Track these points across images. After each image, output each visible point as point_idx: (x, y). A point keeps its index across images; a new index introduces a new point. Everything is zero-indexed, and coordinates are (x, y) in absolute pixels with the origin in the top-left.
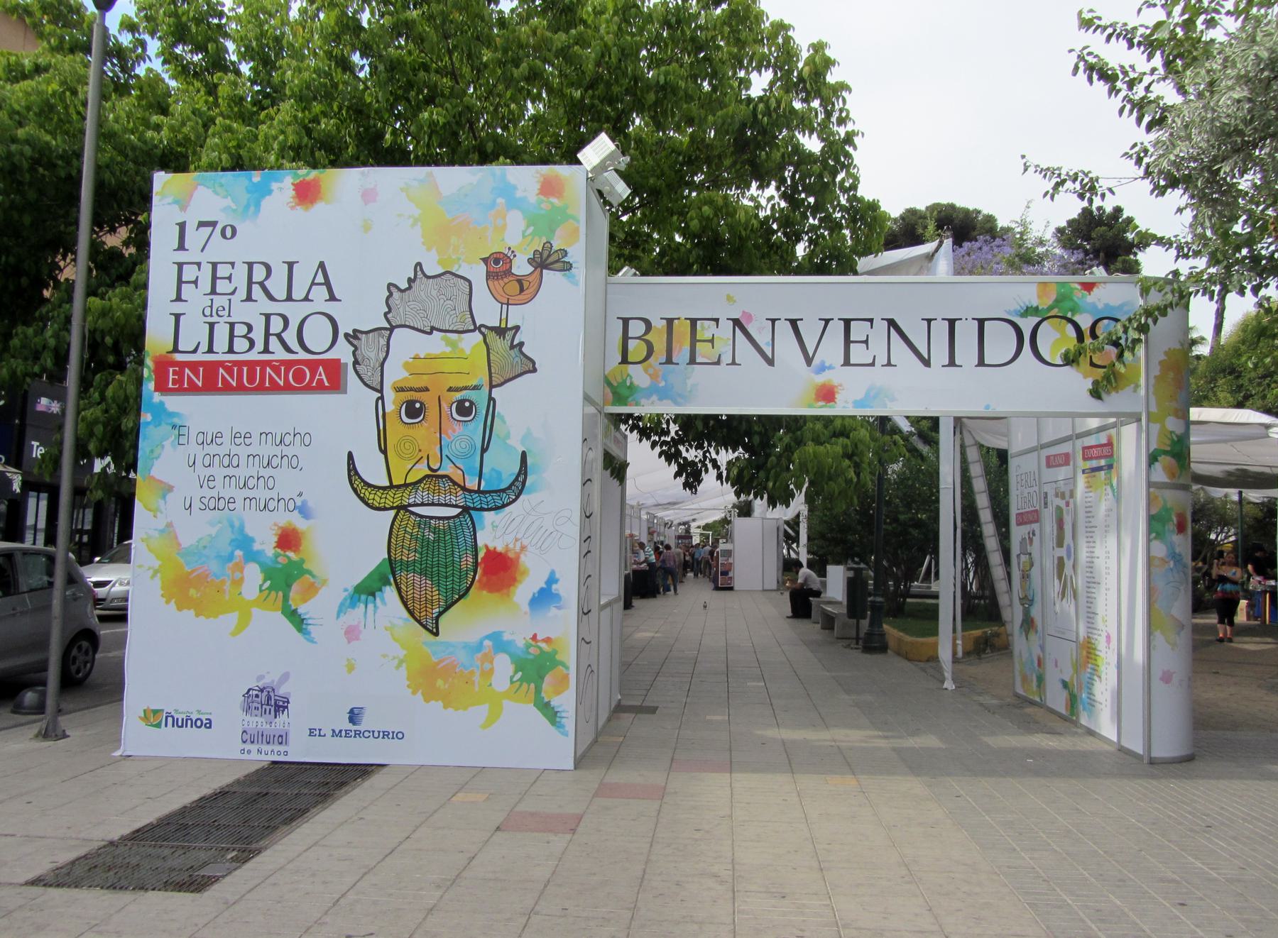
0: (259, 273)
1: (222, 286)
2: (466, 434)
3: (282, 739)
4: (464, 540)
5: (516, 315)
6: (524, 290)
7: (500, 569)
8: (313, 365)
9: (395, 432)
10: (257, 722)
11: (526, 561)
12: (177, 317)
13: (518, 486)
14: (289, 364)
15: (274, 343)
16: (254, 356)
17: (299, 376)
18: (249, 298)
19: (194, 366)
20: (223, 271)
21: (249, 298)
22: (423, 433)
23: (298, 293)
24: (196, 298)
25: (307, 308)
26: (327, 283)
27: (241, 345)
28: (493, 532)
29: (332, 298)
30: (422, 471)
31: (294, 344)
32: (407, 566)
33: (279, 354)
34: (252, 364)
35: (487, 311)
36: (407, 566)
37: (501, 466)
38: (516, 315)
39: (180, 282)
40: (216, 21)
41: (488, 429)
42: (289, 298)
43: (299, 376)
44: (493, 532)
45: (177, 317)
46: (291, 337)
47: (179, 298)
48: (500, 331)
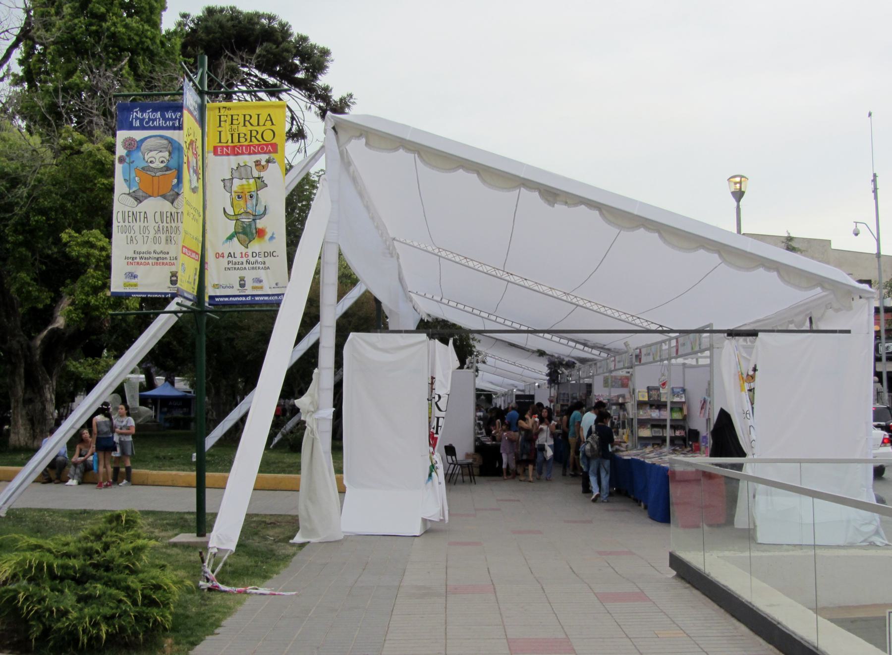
0: (248, 118)
1: (234, 122)
2: (251, 203)
3: (262, 288)
4: (253, 226)
5: (262, 174)
6: (264, 168)
7: (261, 233)
8: (267, 145)
9: (235, 202)
10: (256, 285)
11: (267, 230)
12: (220, 132)
13: (264, 213)
14: (259, 145)
15: (253, 139)
16: (246, 143)
17: (262, 149)
18: (245, 125)
19: (227, 147)
20: (235, 117)
21: (245, 125)
22: (242, 202)
23: (261, 123)
24: (226, 126)
25: (263, 128)
26: (271, 120)
27: (242, 140)
28: (260, 224)
29: (273, 124)
30: (242, 211)
31: (260, 139)
32: (239, 233)
33: (255, 142)
34: (247, 146)
35: (256, 174)
36: (239, 233)
37: (260, 209)
38: (262, 174)
39: (220, 121)
40: (95, 337)
41: (257, 200)
42: (258, 125)
43: (262, 149)
44: (260, 224)
45: (220, 132)
46: (259, 137)
47: (220, 126)
48: (259, 178)
